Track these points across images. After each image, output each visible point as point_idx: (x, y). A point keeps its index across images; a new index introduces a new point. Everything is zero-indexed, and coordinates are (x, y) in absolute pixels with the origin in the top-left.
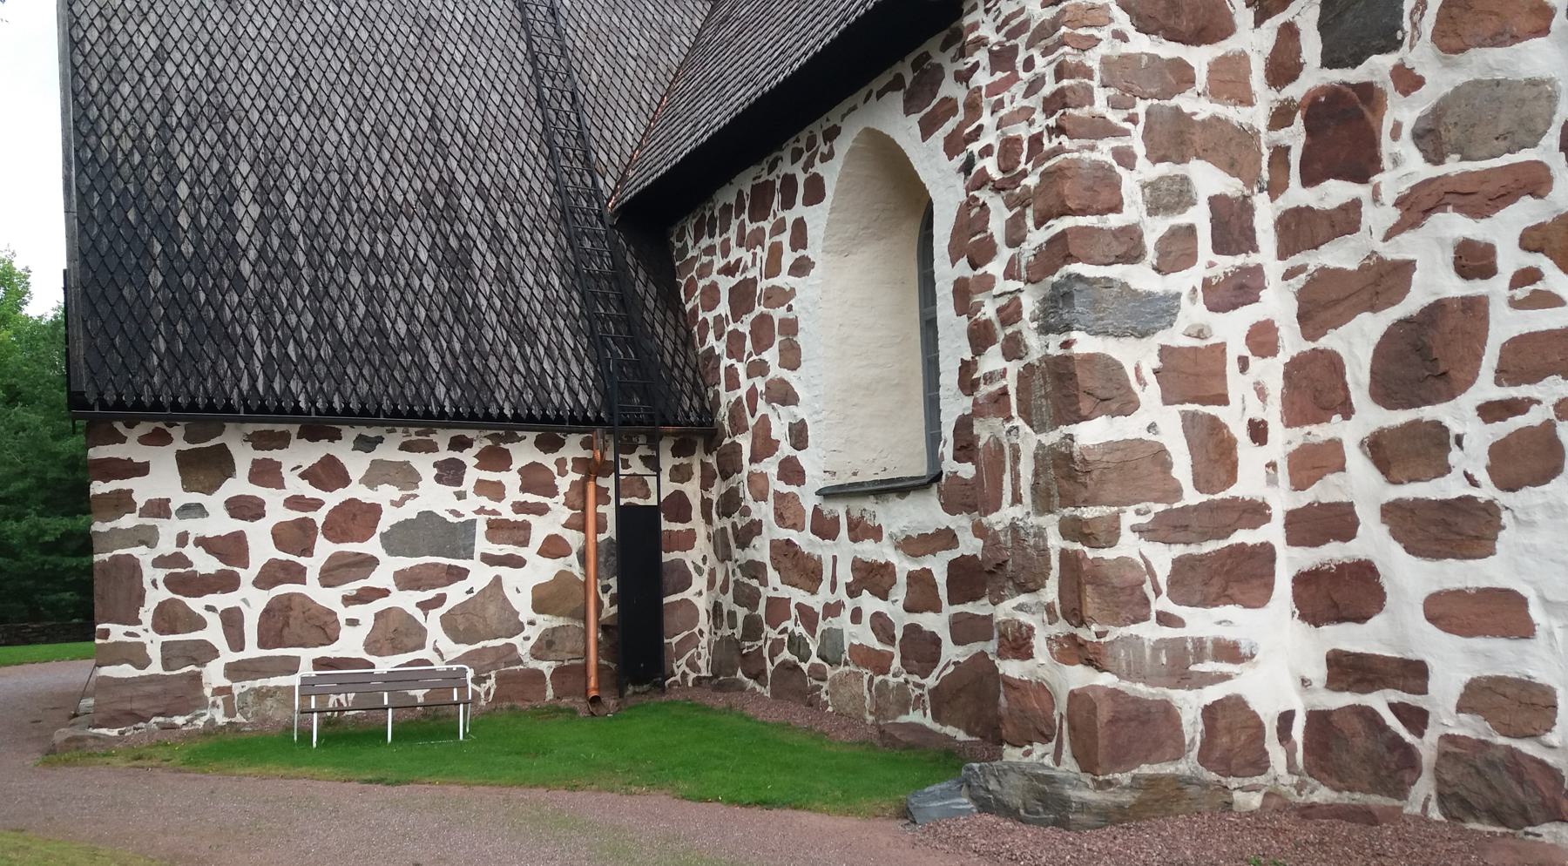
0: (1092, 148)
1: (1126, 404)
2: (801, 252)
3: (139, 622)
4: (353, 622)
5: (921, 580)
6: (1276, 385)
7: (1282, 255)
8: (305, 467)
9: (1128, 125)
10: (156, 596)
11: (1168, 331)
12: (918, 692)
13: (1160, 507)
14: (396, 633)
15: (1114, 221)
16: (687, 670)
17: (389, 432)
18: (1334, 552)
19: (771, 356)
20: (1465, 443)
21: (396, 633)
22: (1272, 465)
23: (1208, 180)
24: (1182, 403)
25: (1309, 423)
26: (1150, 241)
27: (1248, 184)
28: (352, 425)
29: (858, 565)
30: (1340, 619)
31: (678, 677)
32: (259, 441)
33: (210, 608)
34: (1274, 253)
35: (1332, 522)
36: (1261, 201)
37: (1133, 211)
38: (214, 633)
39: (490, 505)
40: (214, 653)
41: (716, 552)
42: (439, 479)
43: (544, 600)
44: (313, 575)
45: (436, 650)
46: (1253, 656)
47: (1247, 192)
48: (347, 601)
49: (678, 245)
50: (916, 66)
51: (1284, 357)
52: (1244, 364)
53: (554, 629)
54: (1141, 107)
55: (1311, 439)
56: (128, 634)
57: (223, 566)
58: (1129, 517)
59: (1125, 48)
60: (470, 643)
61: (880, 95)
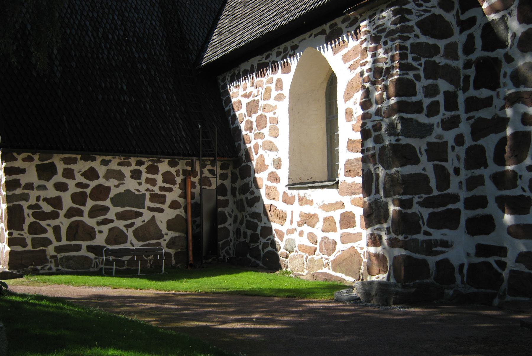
0: (407, 74)
1: (416, 161)
2: (279, 92)
3: (23, 230)
4: (101, 232)
5: (329, 220)
6: (463, 156)
7: (467, 112)
8: (83, 171)
9: (419, 67)
10: (29, 220)
11: (429, 137)
12: (327, 261)
13: (425, 196)
14: (116, 236)
15: (414, 99)
16: (225, 254)
17: (114, 158)
18: (480, 212)
19: (265, 131)
20: (522, 178)
21: (116, 236)
22: (461, 183)
23: (444, 85)
24: (433, 161)
25: (473, 169)
26: (425, 106)
27: (456, 87)
28: (100, 155)
29: (303, 214)
30: (481, 234)
31: (222, 257)
32: (67, 161)
33: (49, 225)
34: (464, 111)
35: (482, 202)
36: (460, 93)
37: (419, 96)
38: (50, 235)
39: (151, 188)
40: (50, 242)
41: (237, 208)
42: (132, 177)
43: (171, 225)
44: (86, 214)
45: (131, 244)
46: (452, 245)
47: (456, 90)
48: (99, 224)
49: (222, 84)
50: (331, 27)
51: (466, 146)
52: (453, 148)
53: (175, 237)
54: (423, 61)
55: (474, 174)
56: (19, 234)
57: (53, 209)
58: (416, 199)
59: (418, 41)
60: (144, 241)
61: (316, 35)
